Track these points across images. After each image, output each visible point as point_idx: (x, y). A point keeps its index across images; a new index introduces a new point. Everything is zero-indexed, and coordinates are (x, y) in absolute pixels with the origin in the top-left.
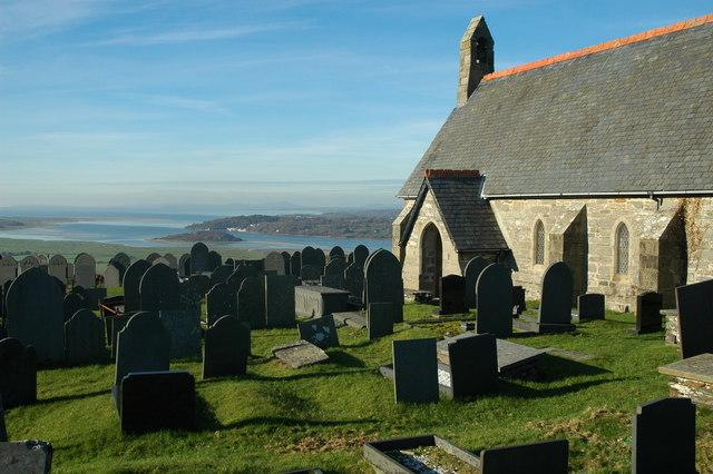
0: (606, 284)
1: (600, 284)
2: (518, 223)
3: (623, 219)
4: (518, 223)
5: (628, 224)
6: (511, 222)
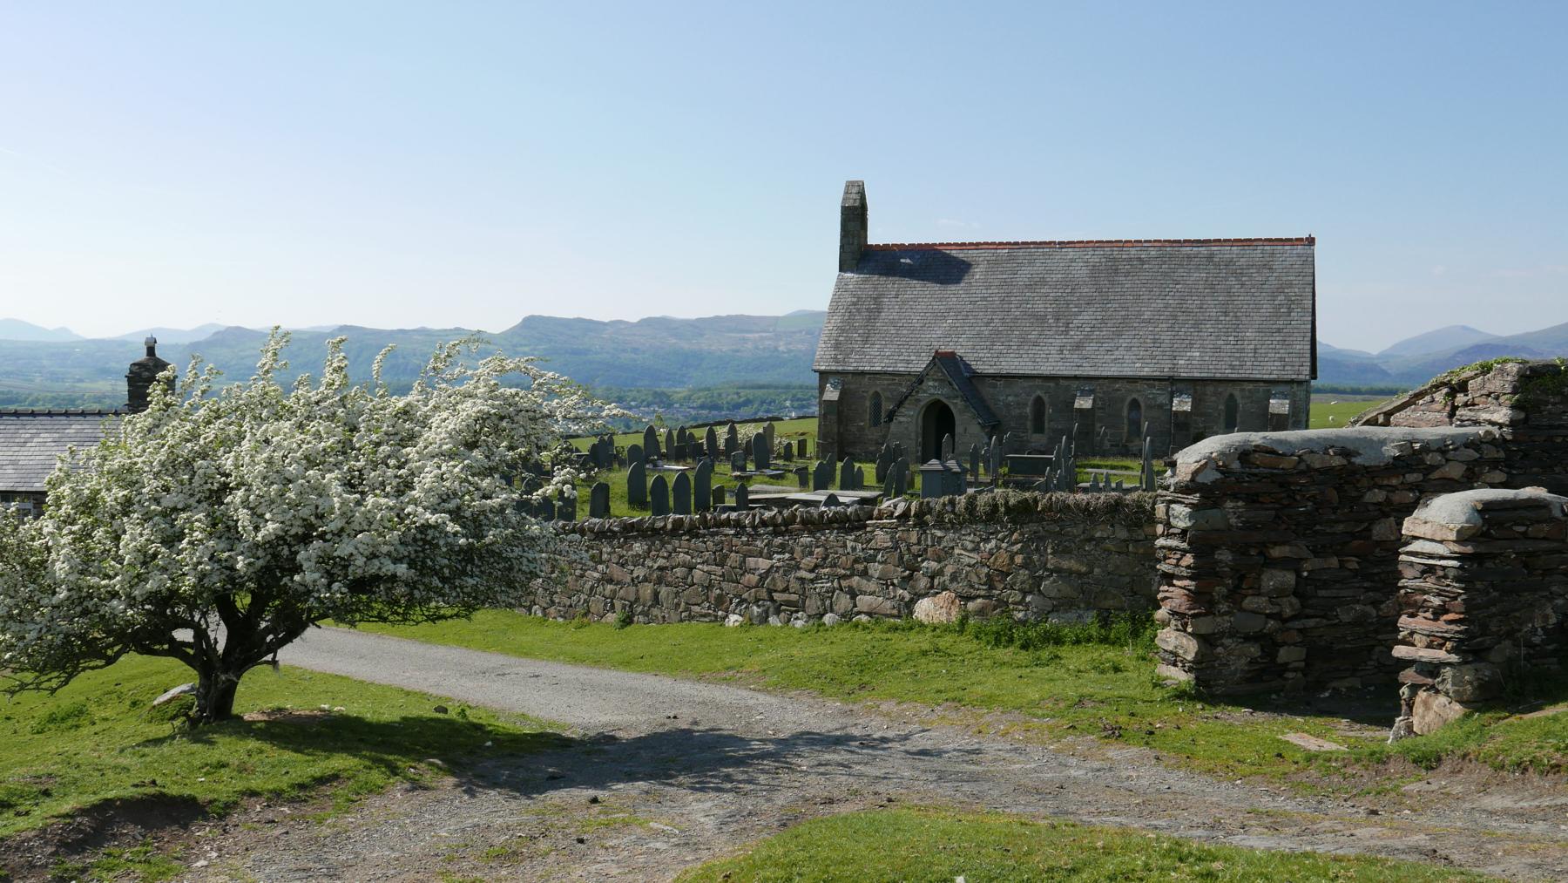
0: (1118, 445)
1: (1112, 445)
2: (1010, 398)
3: (1135, 396)
4: (1010, 398)
5: (1141, 400)
6: (1001, 398)
